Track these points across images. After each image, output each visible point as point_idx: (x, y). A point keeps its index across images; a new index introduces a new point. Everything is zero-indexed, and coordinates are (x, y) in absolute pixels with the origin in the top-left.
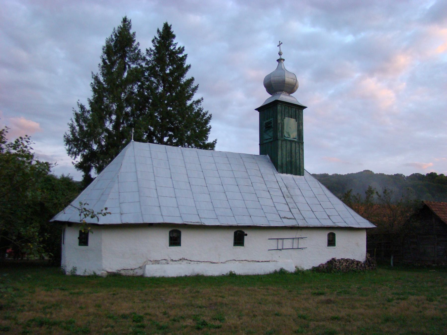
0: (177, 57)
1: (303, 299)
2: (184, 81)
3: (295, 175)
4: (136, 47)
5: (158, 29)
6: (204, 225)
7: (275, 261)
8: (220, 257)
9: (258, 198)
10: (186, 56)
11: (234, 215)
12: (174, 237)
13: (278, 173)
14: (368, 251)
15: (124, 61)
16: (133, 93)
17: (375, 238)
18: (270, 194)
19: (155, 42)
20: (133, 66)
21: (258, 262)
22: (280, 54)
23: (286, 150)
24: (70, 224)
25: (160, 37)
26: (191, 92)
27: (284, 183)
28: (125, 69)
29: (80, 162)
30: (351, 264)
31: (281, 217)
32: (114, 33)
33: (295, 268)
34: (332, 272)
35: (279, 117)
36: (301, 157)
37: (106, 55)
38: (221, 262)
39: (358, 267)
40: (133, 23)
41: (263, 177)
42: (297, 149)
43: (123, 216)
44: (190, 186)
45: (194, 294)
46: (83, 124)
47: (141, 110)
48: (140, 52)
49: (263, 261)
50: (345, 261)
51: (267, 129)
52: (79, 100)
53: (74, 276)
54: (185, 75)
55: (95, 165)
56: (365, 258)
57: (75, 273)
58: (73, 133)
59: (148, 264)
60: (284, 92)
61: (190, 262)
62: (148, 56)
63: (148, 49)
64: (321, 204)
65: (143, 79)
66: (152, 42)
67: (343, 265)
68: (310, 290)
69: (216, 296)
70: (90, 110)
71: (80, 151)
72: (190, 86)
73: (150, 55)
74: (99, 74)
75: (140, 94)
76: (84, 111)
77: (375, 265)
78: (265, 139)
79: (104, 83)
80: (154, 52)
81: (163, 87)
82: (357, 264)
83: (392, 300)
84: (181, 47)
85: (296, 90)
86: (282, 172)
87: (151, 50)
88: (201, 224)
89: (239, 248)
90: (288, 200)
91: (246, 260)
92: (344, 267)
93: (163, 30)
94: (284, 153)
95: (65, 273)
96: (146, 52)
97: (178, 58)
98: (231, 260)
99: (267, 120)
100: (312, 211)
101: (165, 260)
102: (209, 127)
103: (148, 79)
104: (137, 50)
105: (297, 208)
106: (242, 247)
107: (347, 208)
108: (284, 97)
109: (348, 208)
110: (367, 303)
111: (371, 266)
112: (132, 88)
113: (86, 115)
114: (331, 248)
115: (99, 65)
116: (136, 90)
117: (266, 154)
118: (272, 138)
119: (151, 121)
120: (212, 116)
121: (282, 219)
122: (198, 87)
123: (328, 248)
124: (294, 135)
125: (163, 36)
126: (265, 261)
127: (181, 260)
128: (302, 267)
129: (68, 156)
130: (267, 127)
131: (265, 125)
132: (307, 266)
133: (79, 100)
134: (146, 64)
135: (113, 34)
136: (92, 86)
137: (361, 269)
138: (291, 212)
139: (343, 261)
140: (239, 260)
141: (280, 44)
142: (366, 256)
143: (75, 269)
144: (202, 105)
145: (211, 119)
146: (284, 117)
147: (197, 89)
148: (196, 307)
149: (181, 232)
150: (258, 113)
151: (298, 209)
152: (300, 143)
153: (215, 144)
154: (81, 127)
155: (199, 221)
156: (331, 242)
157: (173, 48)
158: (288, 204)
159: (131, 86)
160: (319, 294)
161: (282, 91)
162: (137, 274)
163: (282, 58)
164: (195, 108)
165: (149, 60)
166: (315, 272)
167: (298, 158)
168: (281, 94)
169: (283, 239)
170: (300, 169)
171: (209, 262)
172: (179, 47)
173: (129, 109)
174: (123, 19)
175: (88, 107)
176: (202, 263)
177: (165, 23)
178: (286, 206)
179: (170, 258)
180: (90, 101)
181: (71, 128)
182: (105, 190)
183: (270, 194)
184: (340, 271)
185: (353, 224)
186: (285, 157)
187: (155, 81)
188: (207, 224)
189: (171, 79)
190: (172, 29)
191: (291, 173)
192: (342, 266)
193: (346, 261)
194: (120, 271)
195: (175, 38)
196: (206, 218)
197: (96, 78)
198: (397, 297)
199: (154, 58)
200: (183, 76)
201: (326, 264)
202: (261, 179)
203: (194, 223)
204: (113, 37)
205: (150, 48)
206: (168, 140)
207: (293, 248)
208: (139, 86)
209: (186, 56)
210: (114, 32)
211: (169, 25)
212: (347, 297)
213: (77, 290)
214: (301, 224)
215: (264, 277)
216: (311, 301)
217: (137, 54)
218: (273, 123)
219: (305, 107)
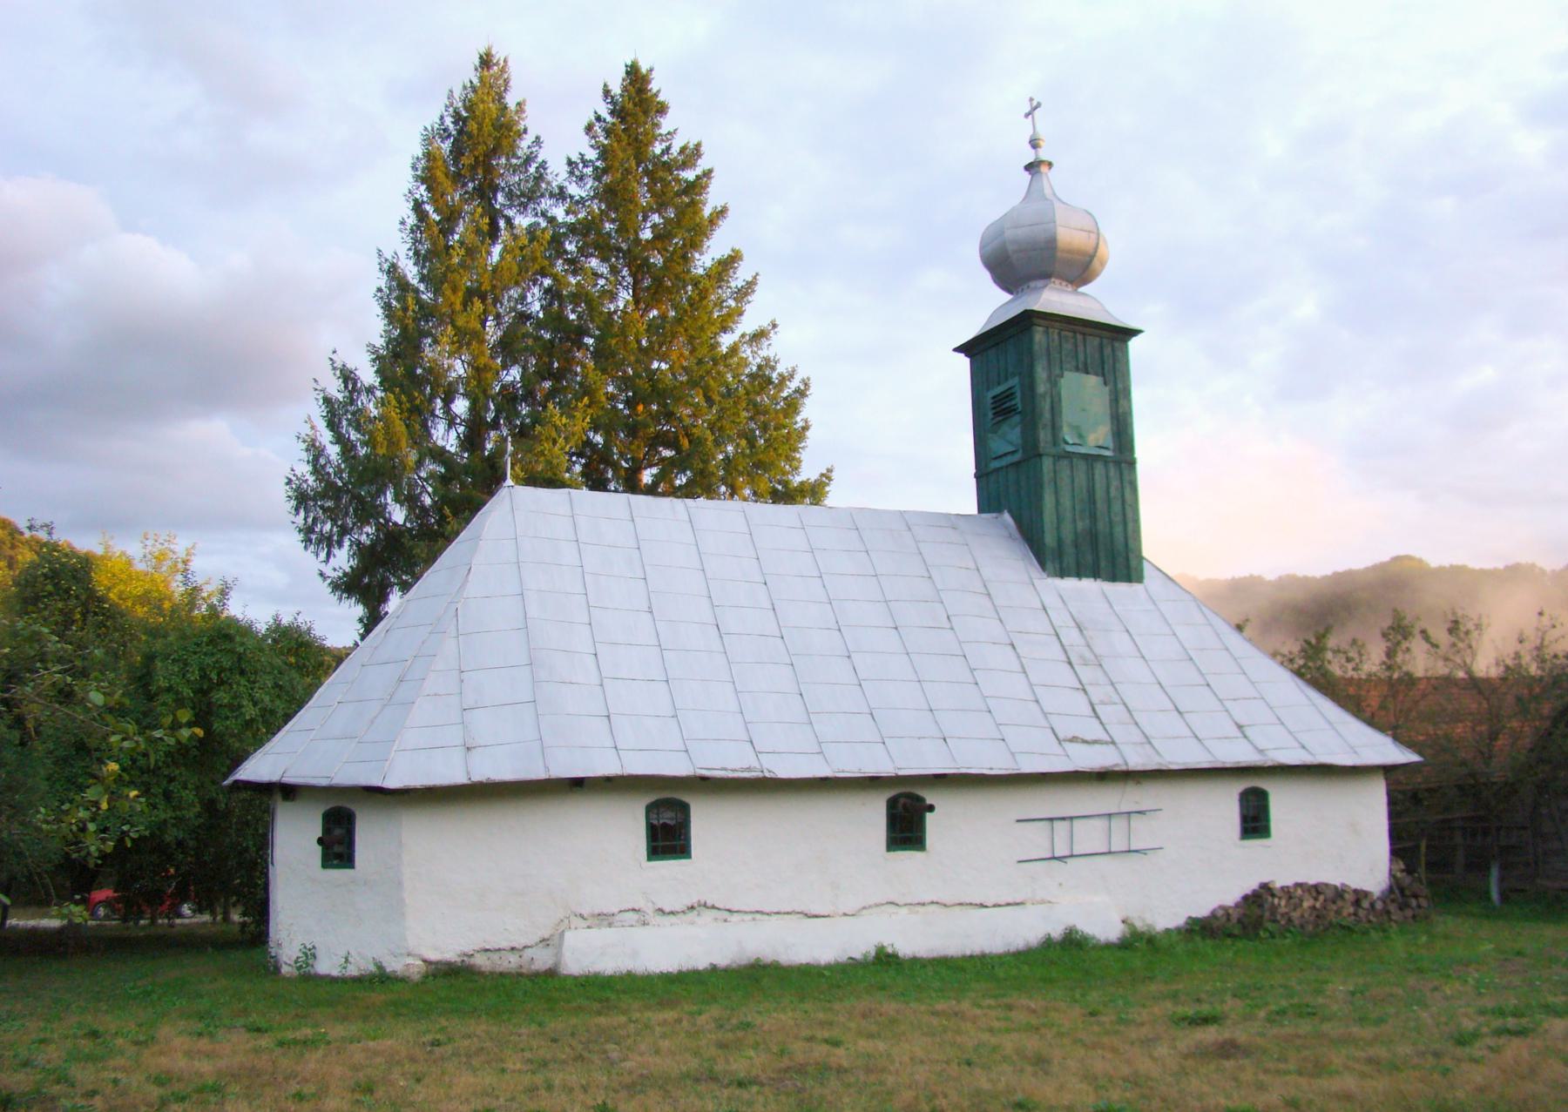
0: (677, 180)
1: (1132, 1044)
2: (706, 265)
3: (491, 494)
4: (531, 153)
6: (771, 779)
9: (972, 670)
10: (708, 174)
11: (883, 738)
12: (665, 825)
13: (1045, 575)
14: (1396, 853)
15: (491, 205)
16: (528, 317)
17: (1426, 803)
18: (1019, 657)
19: (596, 131)
20: (523, 221)
21: (982, 906)
22: (1034, 144)
23: (1073, 497)
24: (289, 791)
25: (612, 113)
26: (732, 303)
27: (1071, 613)
28: (493, 233)
29: (348, 570)
31: (1061, 736)
32: (451, 110)
33: (1122, 926)
34: (1262, 933)
35: (1041, 373)
37: (423, 188)
39: (1361, 913)
40: (514, 72)
41: (989, 595)
42: (1115, 483)
44: (721, 637)
45: (730, 1036)
46: (354, 436)
47: (557, 377)
48: (545, 169)
50: (1309, 891)
51: (1000, 418)
52: (334, 352)
53: (309, 979)
54: (708, 244)
55: (399, 578)
57: (309, 968)
58: (318, 470)
59: (573, 927)
60: (1057, 281)
61: (726, 914)
64: (1212, 686)
65: (560, 266)
66: (587, 134)
67: (1301, 905)
68: (1169, 1005)
69: (811, 1039)
70: (377, 384)
71: (344, 531)
72: (728, 282)
73: (581, 178)
74: (402, 256)
75: (555, 320)
77: (1423, 902)
78: (994, 456)
79: (422, 287)
81: (631, 291)
82: (1357, 903)
83: (1475, 1035)
84: (691, 146)
85: (1102, 270)
86: (1062, 573)
87: (585, 163)
88: (760, 775)
90: (1086, 674)
91: (937, 903)
93: (625, 89)
94: (1066, 502)
95: (277, 969)
96: (567, 168)
97: (681, 185)
98: (877, 905)
99: (999, 384)
101: (634, 910)
102: (801, 424)
103: (574, 265)
104: (536, 165)
105: (1118, 700)
108: (1054, 299)
109: (1313, 694)
110: (1372, 1052)
111: (1412, 909)
112: (523, 298)
114: (1255, 844)
115: (403, 223)
116: (536, 307)
117: (999, 510)
118: (1021, 451)
119: (590, 411)
120: (813, 384)
121: (1064, 744)
122: (756, 284)
124: (1098, 437)
126: (1008, 904)
127: (692, 908)
130: (998, 409)
133: (334, 352)
134: (567, 213)
136: (381, 298)
137: (1372, 918)
138: (1098, 717)
140: (911, 904)
142: (1390, 870)
143: (310, 954)
146: (1057, 371)
147: (753, 291)
148: (726, 1081)
150: (964, 362)
151: (1125, 704)
153: (828, 484)
154: (347, 447)
155: (755, 764)
156: (1255, 822)
157: (663, 151)
158: (1084, 690)
159: (514, 293)
160: (1199, 1021)
161: (1046, 276)
162: (533, 967)
163: (1044, 158)
164: (751, 359)
165: (577, 198)
166: (1198, 938)
167: (1117, 519)
168: (1045, 286)
169: (1071, 818)
170: (1127, 559)
171: (798, 913)
172: (682, 144)
173: (514, 374)
174: (481, 57)
175: (368, 375)
177: (629, 63)
178: (1080, 696)
179: (653, 903)
181: (307, 450)
182: (409, 662)
183: (1019, 657)
184: (1290, 932)
186: (1068, 515)
187: (604, 269)
188: (783, 773)
189: (657, 259)
190: (653, 82)
191: (1096, 574)
193: (1314, 894)
195: (668, 115)
196: (777, 750)
197: (393, 271)
198: (1497, 1023)
199: (597, 188)
200: (702, 247)
201: (1237, 905)
202: (985, 602)
204: (449, 121)
205: (580, 154)
206: (657, 480)
207: (1110, 853)
208: (548, 291)
209: (708, 174)
210: (452, 104)
211: (644, 70)
212: (1301, 1031)
213: (307, 1032)
214: (1137, 760)
215: (1002, 964)
216: (1162, 1050)
217: (535, 178)
218: (1018, 394)
219: (1133, 332)
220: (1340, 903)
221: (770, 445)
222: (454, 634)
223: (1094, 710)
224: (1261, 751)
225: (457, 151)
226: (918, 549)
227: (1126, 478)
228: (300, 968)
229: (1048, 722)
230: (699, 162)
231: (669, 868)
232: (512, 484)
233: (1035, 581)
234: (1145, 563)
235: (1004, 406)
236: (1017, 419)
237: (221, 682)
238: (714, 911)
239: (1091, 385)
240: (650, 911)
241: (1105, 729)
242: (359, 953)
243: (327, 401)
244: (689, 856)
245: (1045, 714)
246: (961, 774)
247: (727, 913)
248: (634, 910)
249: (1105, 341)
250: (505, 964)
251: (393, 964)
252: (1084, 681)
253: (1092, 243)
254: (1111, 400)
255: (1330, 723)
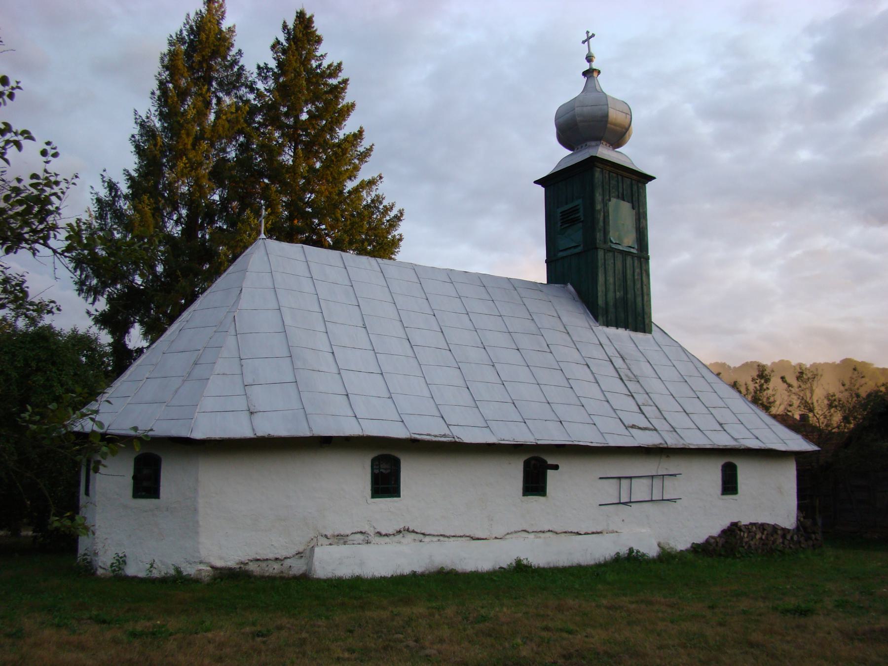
0: (325, 84)
5: (285, 22)
6: (460, 443)
7: (614, 532)
8: (492, 525)
9: (568, 379)
10: (345, 81)
13: (598, 325)
14: (800, 507)
21: (578, 534)
22: (589, 59)
23: (615, 272)
24: (113, 441)
25: (288, 40)
30: (772, 536)
31: (626, 424)
32: (188, 27)
35: (598, 197)
36: (645, 290)
38: (495, 536)
39: (786, 542)
42: (637, 270)
43: (258, 419)
44: (412, 347)
49: (588, 532)
52: (105, 171)
56: (796, 522)
60: (604, 143)
62: (260, 81)
63: (262, 66)
64: (700, 398)
66: (272, 50)
67: (755, 537)
71: (105, 285)
75: (244, 162)
76: (116, 195)
80: (274, 74)
82: (784, 537)
84: (335, 64)
86: (607, 325)
89: (535, 501)
90: (632, 386)
91: (551, 531)
92: (757, 543)
94: (611, 280)
95: (94, 574)
99: (567, 204)
100: (685, 412)
105: (652, 404)
106: (541, 499)
107: (752, 408)
108: (604, 152)
113: (120, 206)
115: (153, 93)
118: (582, 246)
123: (723, 499)
124: (628, 241)
125: (295, 37)
126: (593, 533)
127: (400, 532)
128: (671, 545)
129: (77, 296)
131: (561, 216)
132: (681, 543)
135: (184, 27)
136: (134, 141)
137: (791, 546)
138: (643, 414)
139: (756, 528)
140: (536, 532)
141: (589, 38)
142: (797, 517)
143: (122, 561)
144: (381, 189)
145: (401, 220)
147: (370, 155)
149: (400, 460)
150: (541, 190)
151: (656, 406)
152: (642, 259)
155: (447, 432)
156: (729, 486)
157: (317, 66)
162: (291, 573)
163: (595, 68)
167: (639, 293)
169: (631, 478)
170: (644, 318)
171: (467, 536)
175: (124, 188)
176: (452, 539)
177: (299, 11)
180: (129, 175)
183: (592, 373)
184: (752, 553)
185: (773, 443)
186: (611, 287)
191: (626, 327)
192: (754, 540)
194: (247, 563)
195: (322, 44)
201: (720, 536)
203: (436, 436)
204: (185, 33)
207: (652, 501)
208: (241, 145)
209: (345, 81)
214: (672, 441)
219: (651, 178)
220: (775, 536)
221: (382, 247)
222: (233, 333)
223: (640, 409)
224: (736, 440)
225: (188, 54)
227: (644, 268)
228: (114, 571)
229: (617, 415)
230: (340, 74)
231: (385, 503)
232: (265, 237)
233: (593, 328)
235: (570, 217)
237: (38, 369)
238: (414, 534)
239: (625, 208)
240: (372, 534)
241: (649, 421)
242: (161, 561)
243: (99, 200)
244: (399, 496)
245: (614, 410)
246: (575, 445)
247: (422, 536)
248: (361, 532)
249: (634, 182)
250: (271, 570)
251: (188, 569)
252: (632, 391)
253: (628, 121)
254: (636, 220)
255: (768, 425)
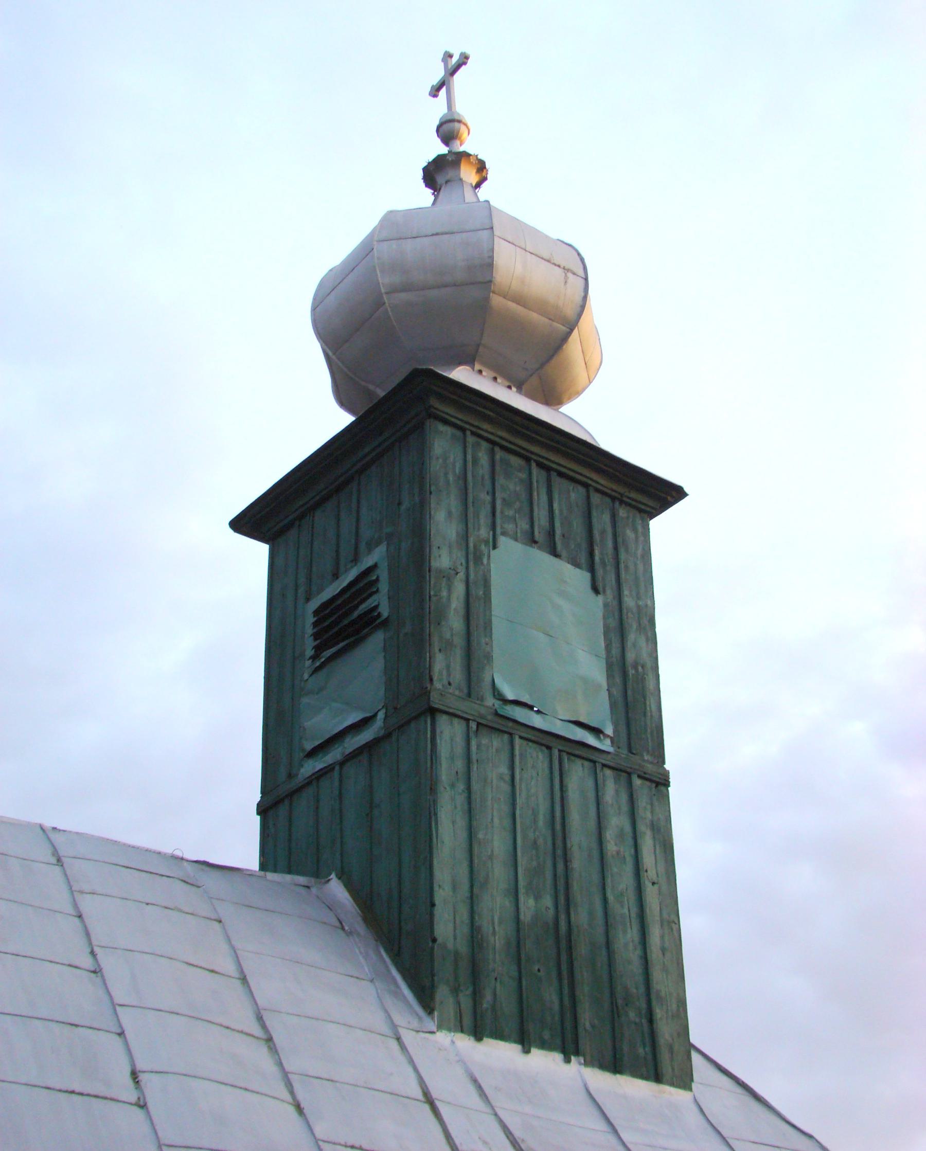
41: (269, 1039)
42: (617, 822)
117: (318, 873)
167: (625, 909)
186: (499, 873)
202: (260, 1056)
226: (75, 905)
227: (645, 813)
233: (408, 1037)
234: (695, 1056)
235: (356, 614)
236: (376, 640)
